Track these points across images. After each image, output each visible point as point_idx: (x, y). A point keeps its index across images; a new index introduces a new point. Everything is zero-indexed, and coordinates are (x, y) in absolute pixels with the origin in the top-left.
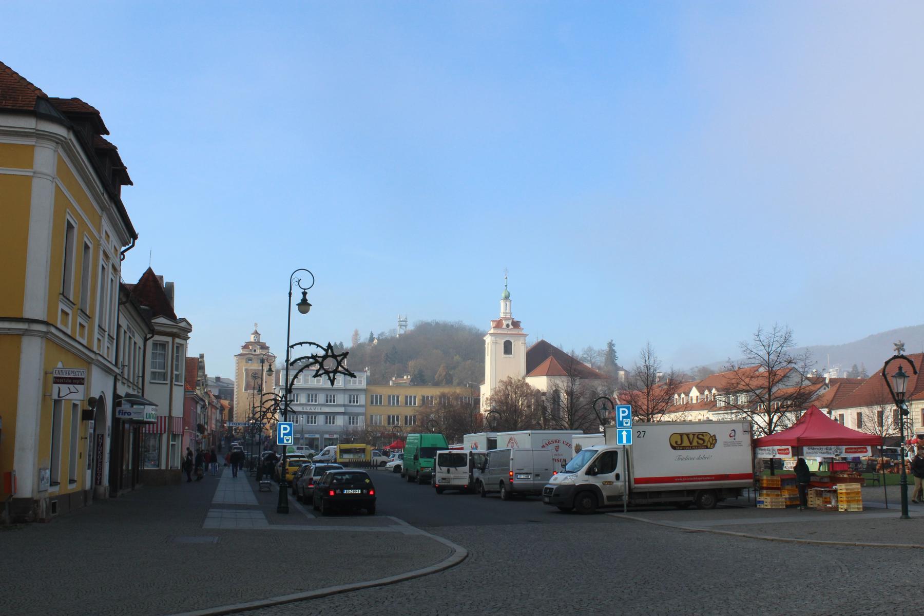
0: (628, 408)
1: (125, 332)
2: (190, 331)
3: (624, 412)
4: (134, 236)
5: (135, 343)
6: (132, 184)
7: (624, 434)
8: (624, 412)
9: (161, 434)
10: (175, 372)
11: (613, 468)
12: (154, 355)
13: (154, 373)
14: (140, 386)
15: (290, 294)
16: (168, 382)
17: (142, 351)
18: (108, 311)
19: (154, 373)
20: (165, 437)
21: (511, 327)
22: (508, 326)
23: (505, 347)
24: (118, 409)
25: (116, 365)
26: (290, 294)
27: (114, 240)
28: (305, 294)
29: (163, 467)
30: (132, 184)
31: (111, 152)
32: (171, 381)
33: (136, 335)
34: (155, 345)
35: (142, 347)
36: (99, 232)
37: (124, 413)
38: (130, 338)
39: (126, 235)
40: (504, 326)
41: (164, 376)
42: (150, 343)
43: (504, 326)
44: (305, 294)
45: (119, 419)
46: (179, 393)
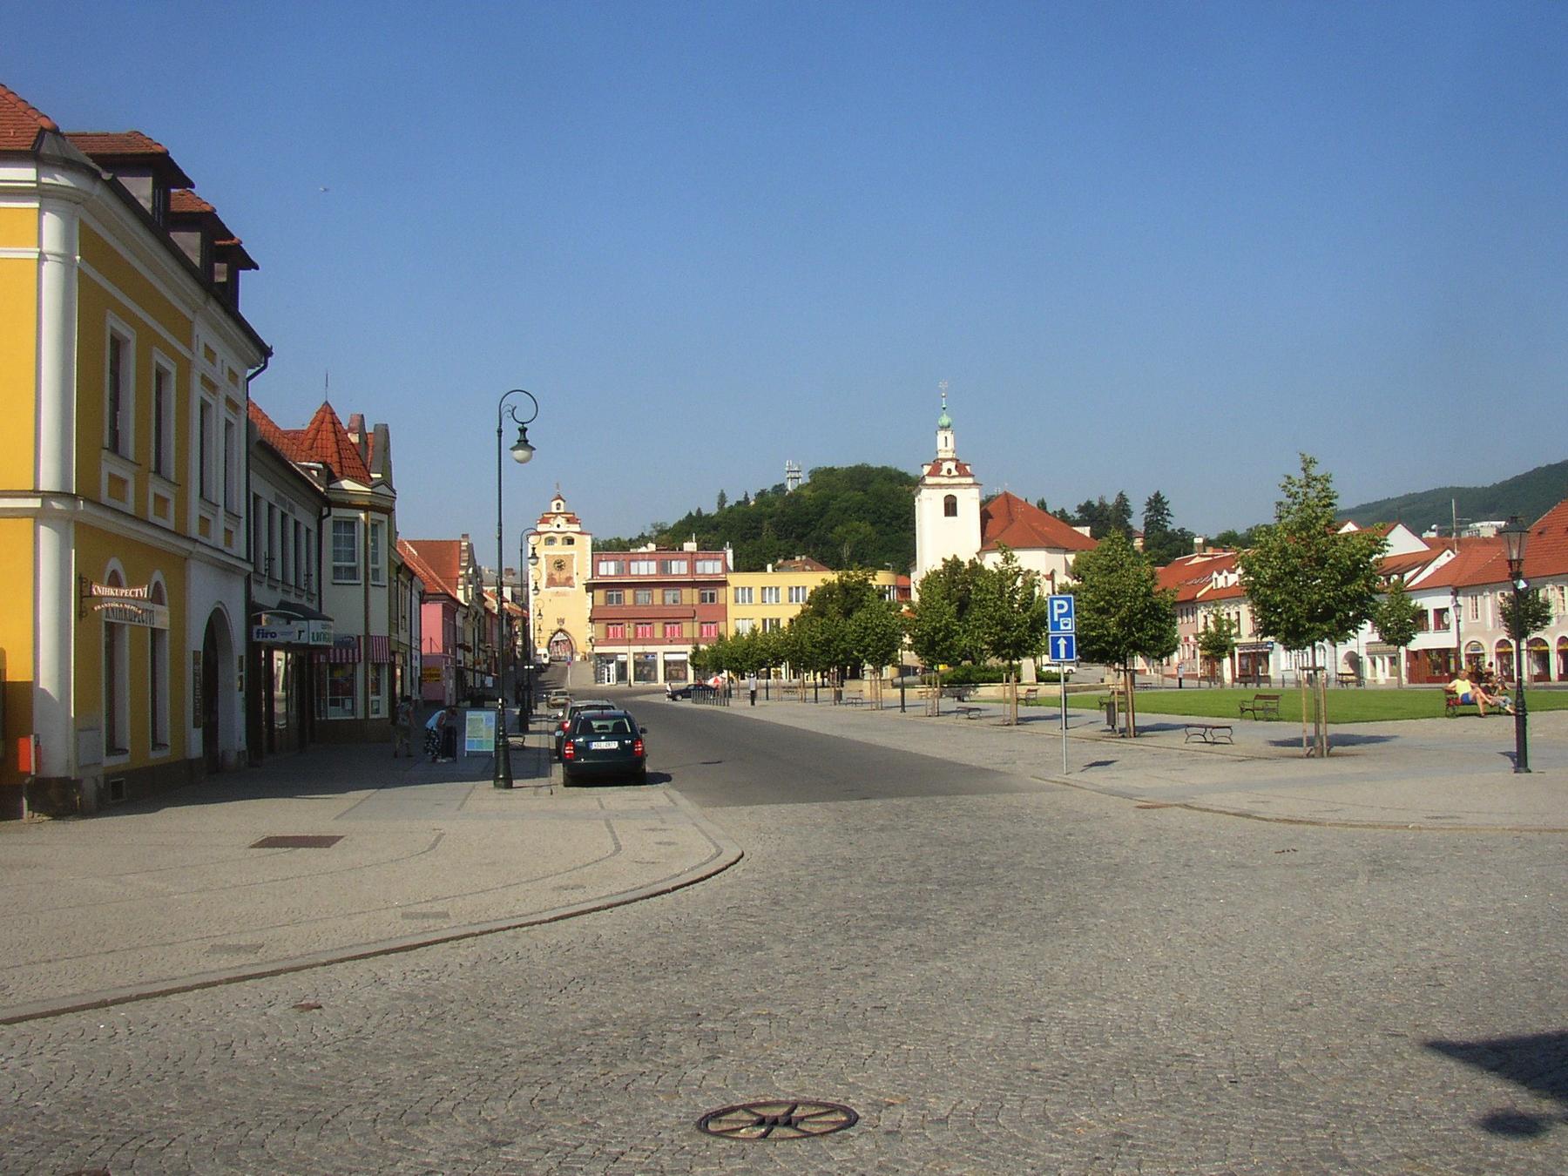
0: (1068, 600)
1: (271, 507)
2: (1089, 504)
3: (1061, 607)
4: (266, 352)
5: (297, 524)
6: (257, 268)
7: (1062, 642)
8: (1061, 607)
9: (354, 664)
10: (371, 566)
11: (1296, 638)
12: (336, 541)
13: (336, 569)
14: (314, 590)
15: (500, 432)
16: (362, 580)
17: (314, 535)
18: (230, 475)
19: (336, 569)
20: (360, 670)
21: (954, 472)
22: (949, 471)
23: (946, 505)
24: (256, 628)
25: (248, 560)
26: (500, 432)
27: (227, 358)
28: (523, 431)
29: (361, 716)
30: (257, 268)
31: (208, 223)
32: (366, 579)
33: (298, 508)
34: (337, 524)
35: (314, 529)
36: (189, 346)
37: (265, 635)
38: (284, 516)
39: (253, 353)
40: (944, 472)
41: (352, 572)
42: (328, 524)
43: (944, 472)
44: (523, 431)
45: (259, 643)
46: (379, 599)
